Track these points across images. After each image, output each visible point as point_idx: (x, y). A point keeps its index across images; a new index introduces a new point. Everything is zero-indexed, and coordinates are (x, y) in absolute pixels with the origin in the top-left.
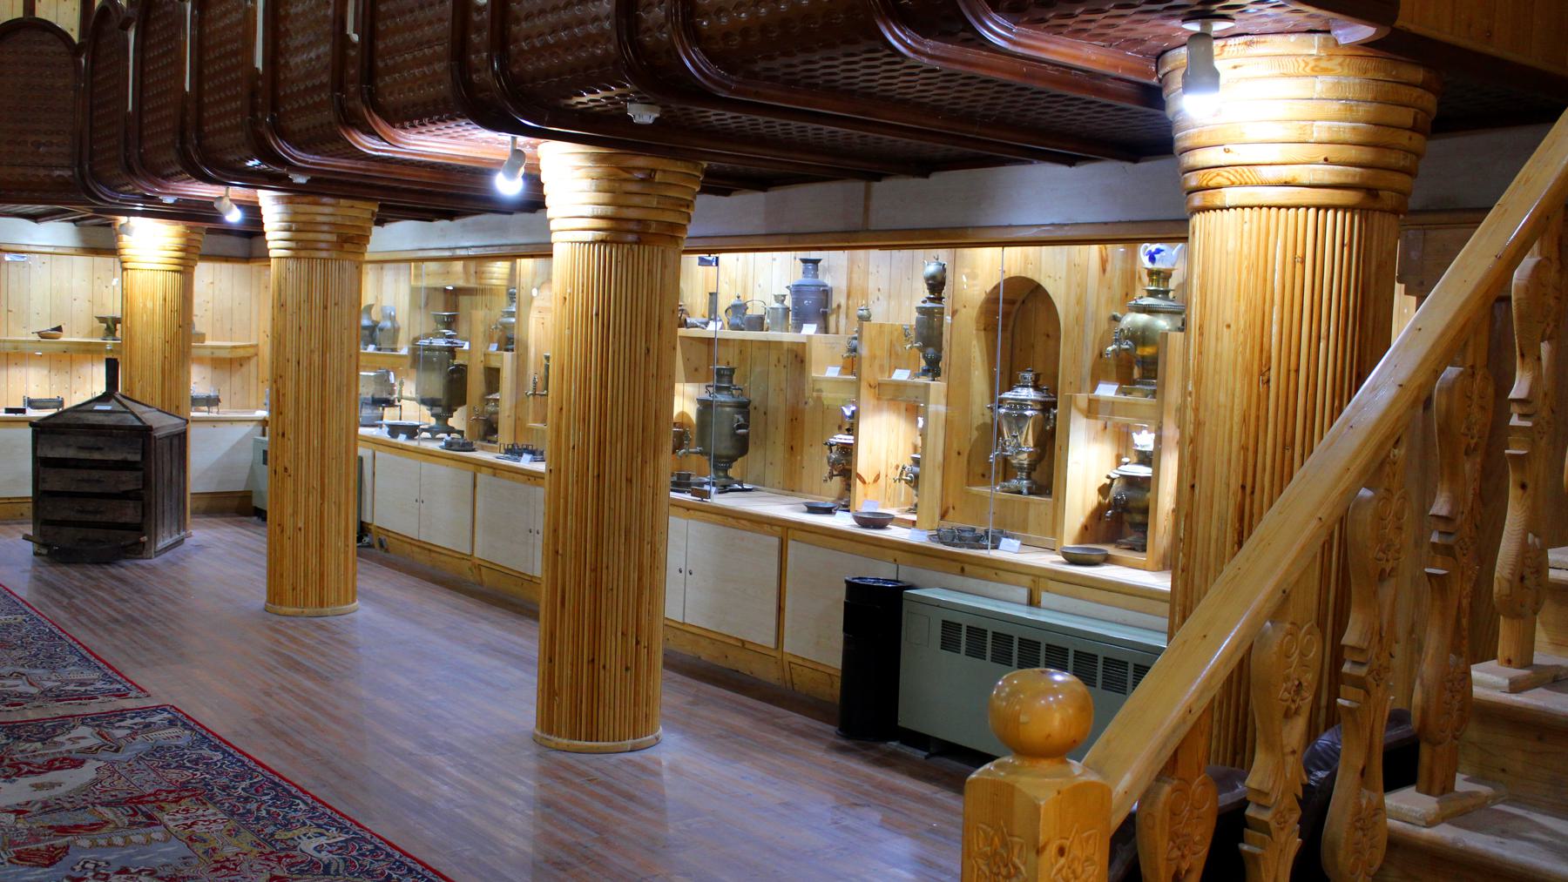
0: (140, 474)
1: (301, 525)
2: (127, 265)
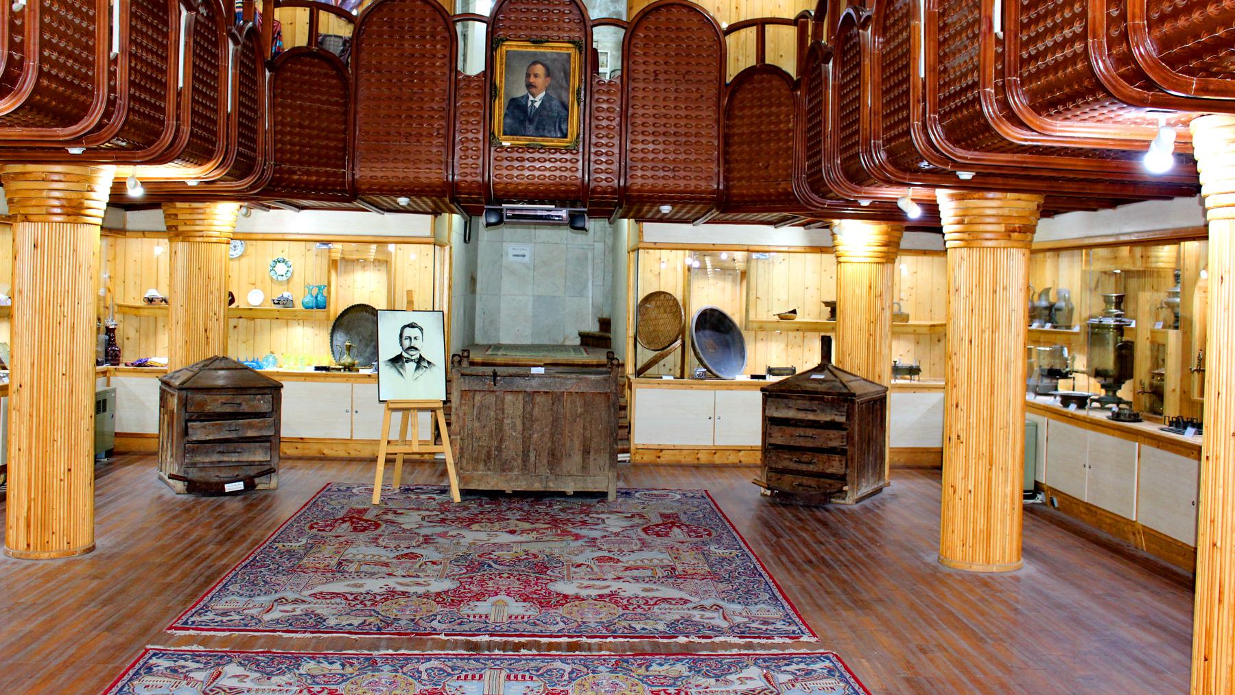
0: (844, 433)
1: (971, 487)
2: (841, 259)
